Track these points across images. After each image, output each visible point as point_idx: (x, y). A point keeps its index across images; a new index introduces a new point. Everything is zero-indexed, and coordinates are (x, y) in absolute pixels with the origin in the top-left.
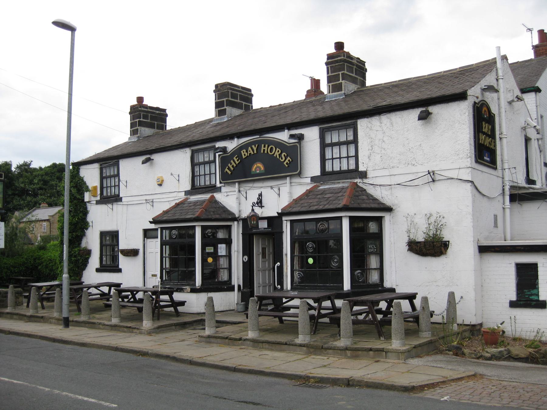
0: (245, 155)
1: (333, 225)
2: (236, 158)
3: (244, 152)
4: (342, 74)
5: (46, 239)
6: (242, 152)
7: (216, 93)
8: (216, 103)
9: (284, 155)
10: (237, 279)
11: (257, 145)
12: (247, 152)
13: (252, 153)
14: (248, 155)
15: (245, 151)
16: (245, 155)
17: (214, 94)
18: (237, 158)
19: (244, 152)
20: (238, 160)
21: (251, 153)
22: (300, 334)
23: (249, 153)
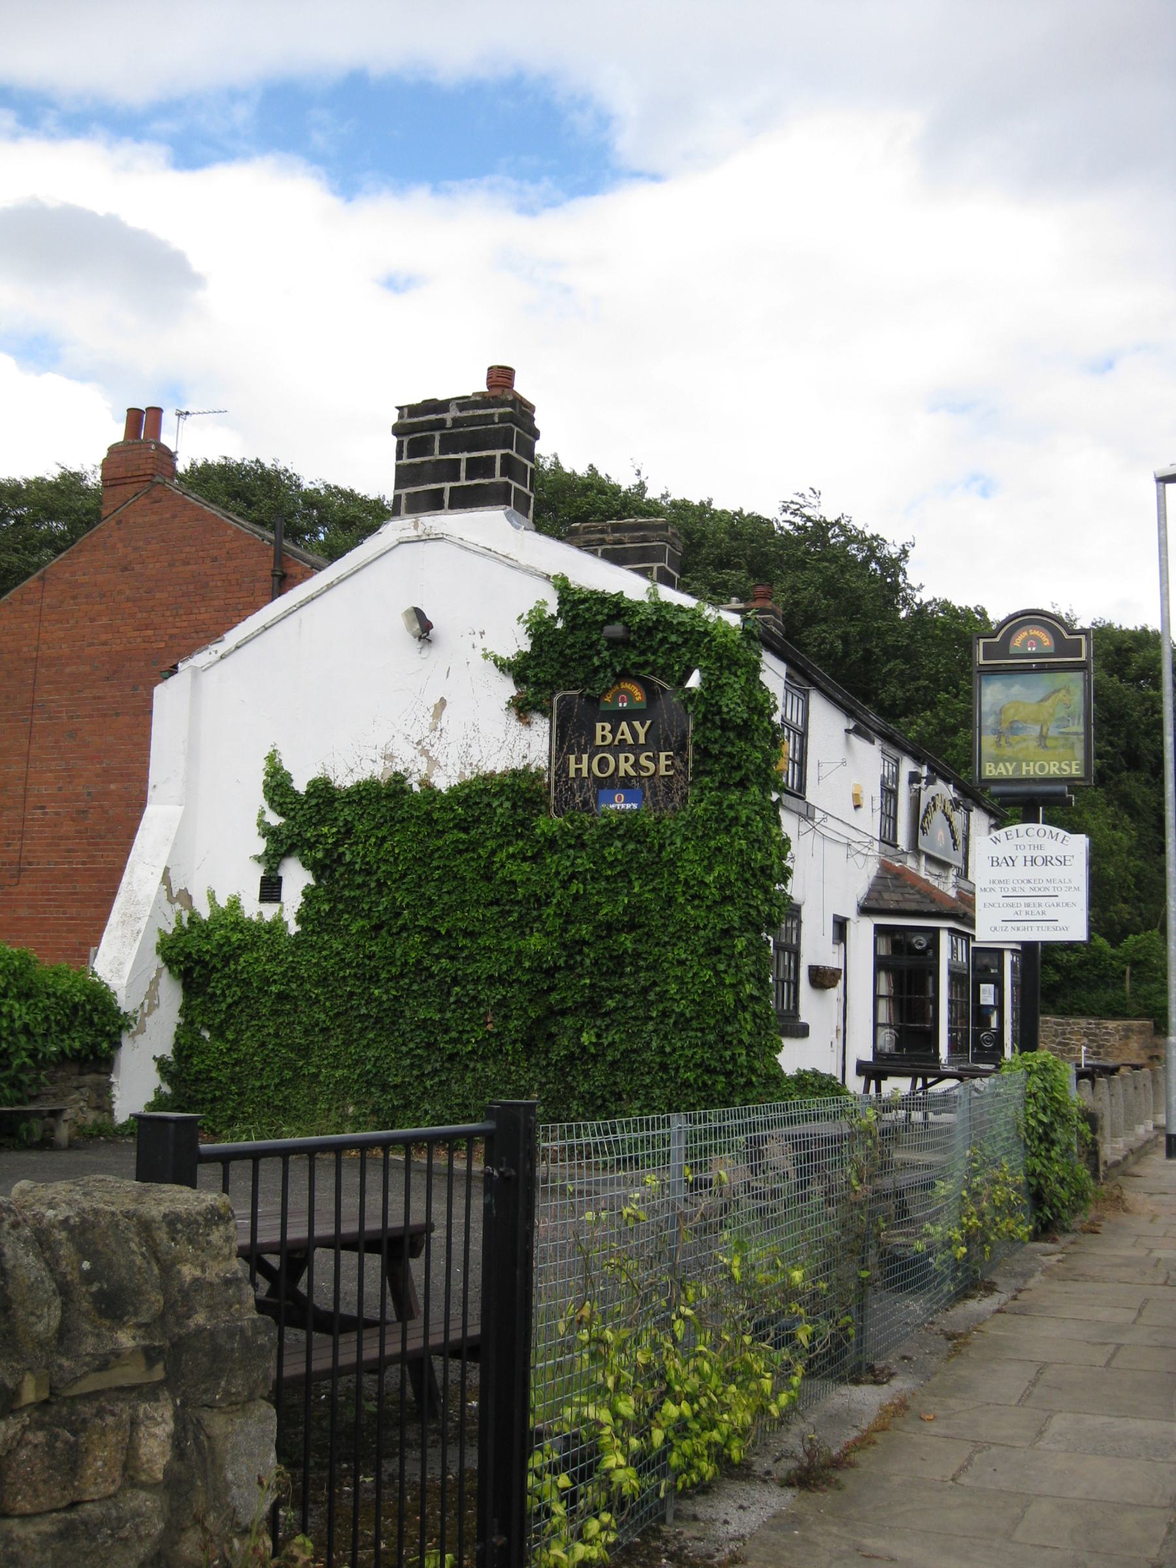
0: (604, 738)
1: (921, 942)
2: (667, 758)
3: (603, 728)
4: (659, 568)
5: (958, 893)
6: (599, 726)
7: (406, 440)
8: (398, 467)
9: (647, 758)
10: (902, 1113)
11: (648, 722)
12: (614, 731)
13: (630, 741)
14: (616, 743)
15: (608, 726)
16: (604, 738)
17: (394, 440)
18: (669, 763)
19: (603, 728)
20: (667, 768)
21: (625, 740)
22: (1076, 734)
23: (619, 737)
